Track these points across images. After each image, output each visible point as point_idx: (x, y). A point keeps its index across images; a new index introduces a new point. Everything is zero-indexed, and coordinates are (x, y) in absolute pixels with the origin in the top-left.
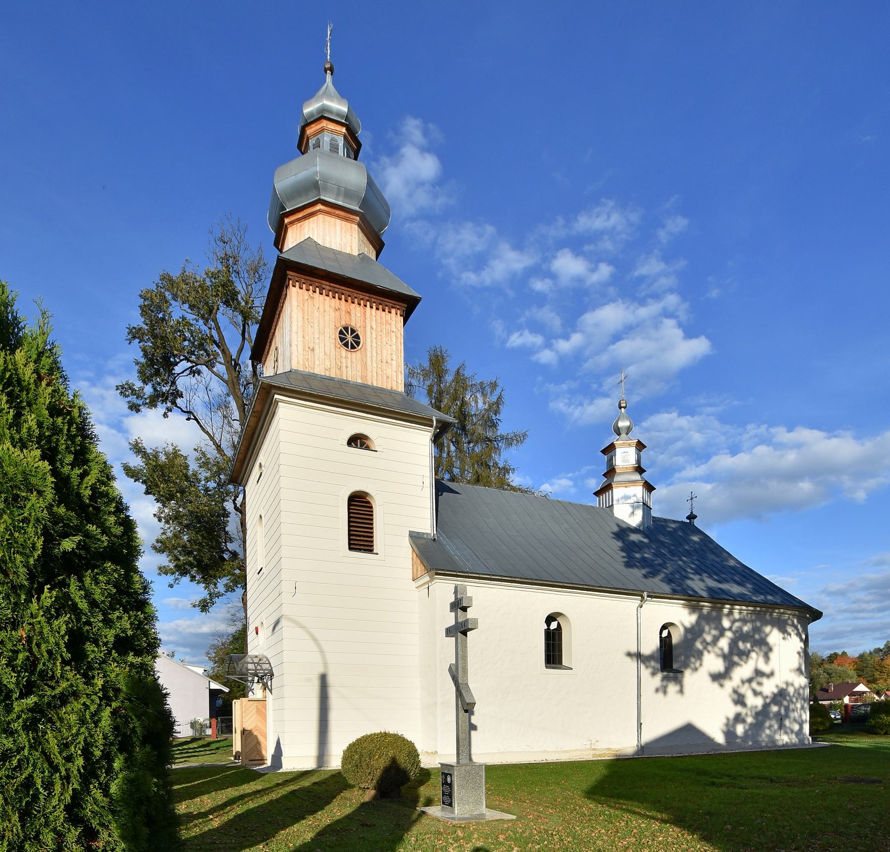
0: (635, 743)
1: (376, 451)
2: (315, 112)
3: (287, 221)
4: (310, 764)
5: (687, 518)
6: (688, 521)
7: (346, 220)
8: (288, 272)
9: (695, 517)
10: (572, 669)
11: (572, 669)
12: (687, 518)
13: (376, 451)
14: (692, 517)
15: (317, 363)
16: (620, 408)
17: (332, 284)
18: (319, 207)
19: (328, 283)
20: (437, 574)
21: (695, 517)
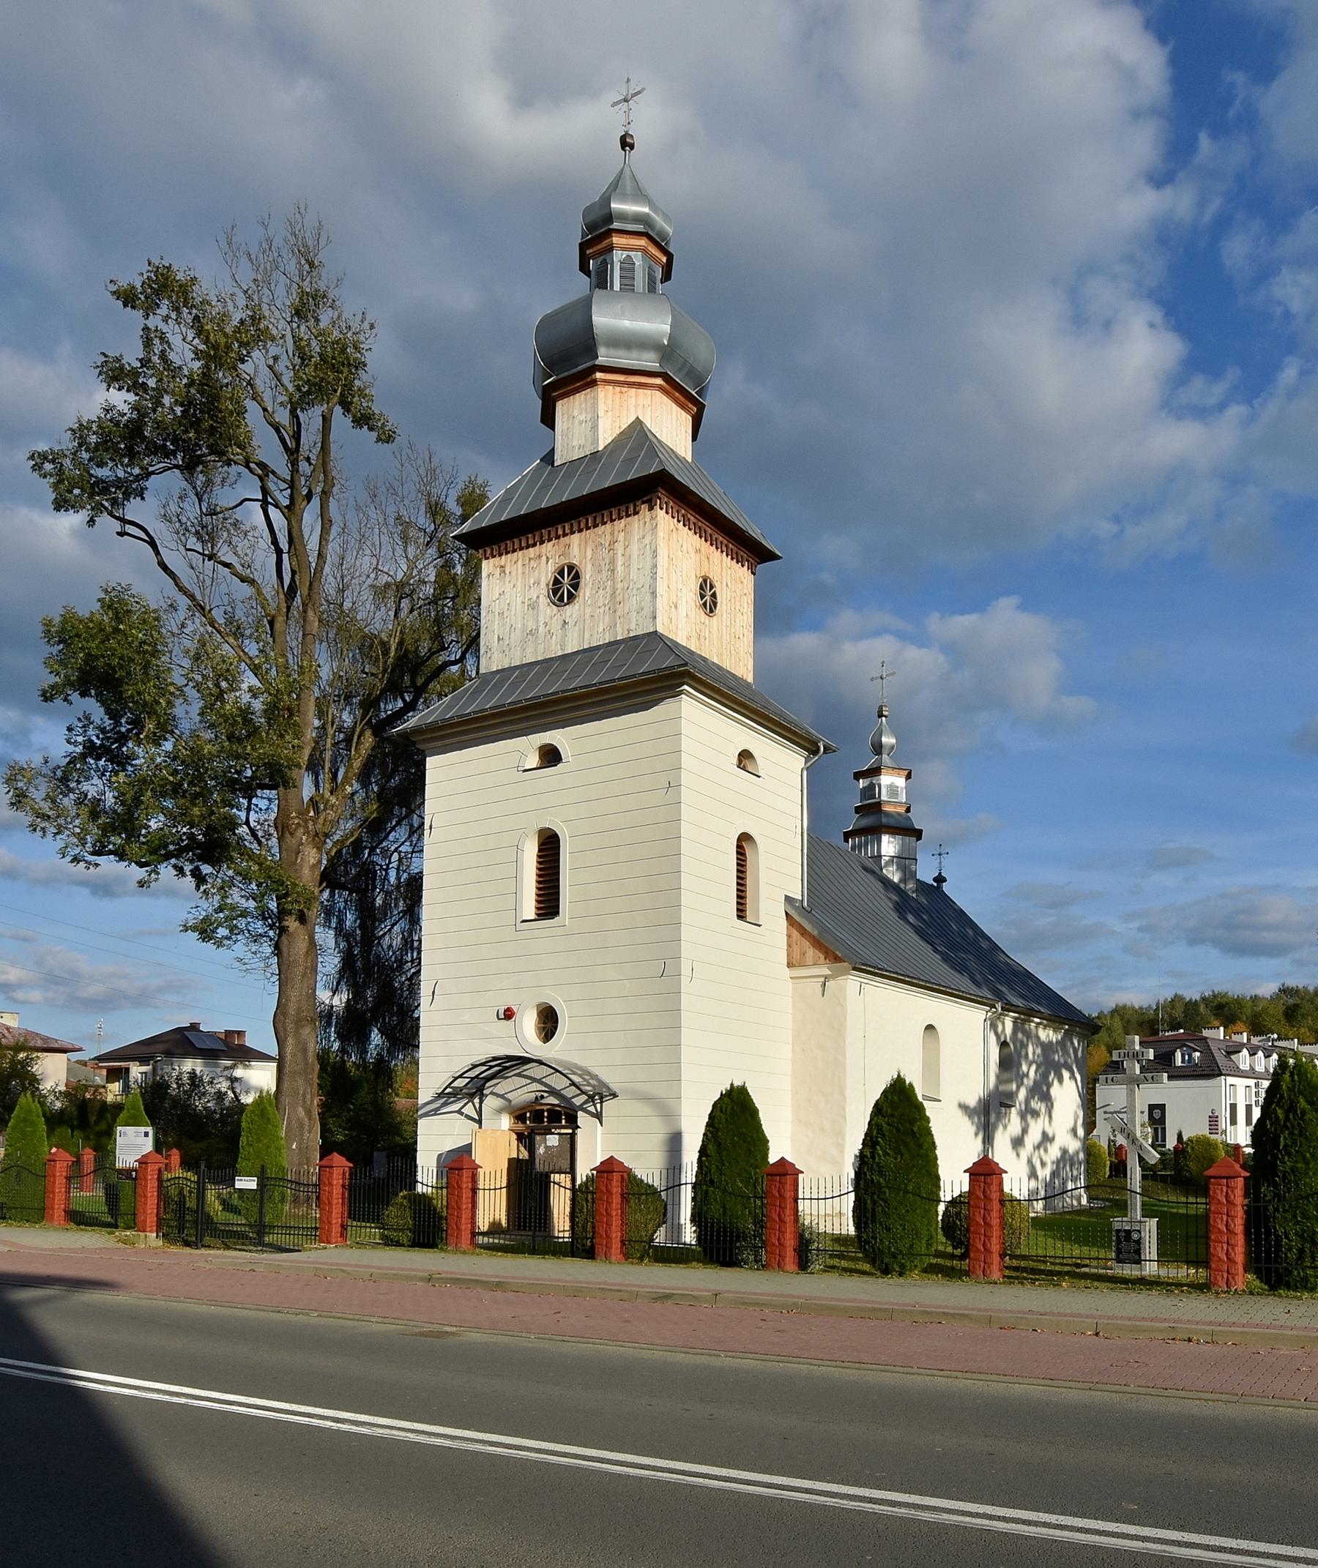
0: (559, 1089)
1: (759, 777)
2: (657, 228)
3: (599, 375)
4: (516, 1156)
5: (935, 880)
6: (935, 884)
7: (682, 406)
8: (660, 489)
9: (945, 880)
10: (940, 1101)
11: (940, 1101)
12: (935, 880)
13: (759, 777)
14: (940, 879)
15: (680, 627)
16: (880, 715)
17: (697, 516)
18: (659, 381)
19: (694, 514)
20: (854, 969)
21: (945, 880)
